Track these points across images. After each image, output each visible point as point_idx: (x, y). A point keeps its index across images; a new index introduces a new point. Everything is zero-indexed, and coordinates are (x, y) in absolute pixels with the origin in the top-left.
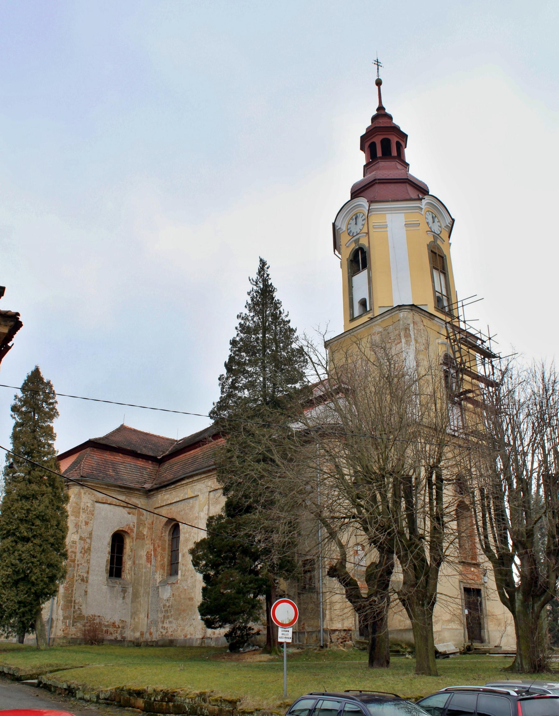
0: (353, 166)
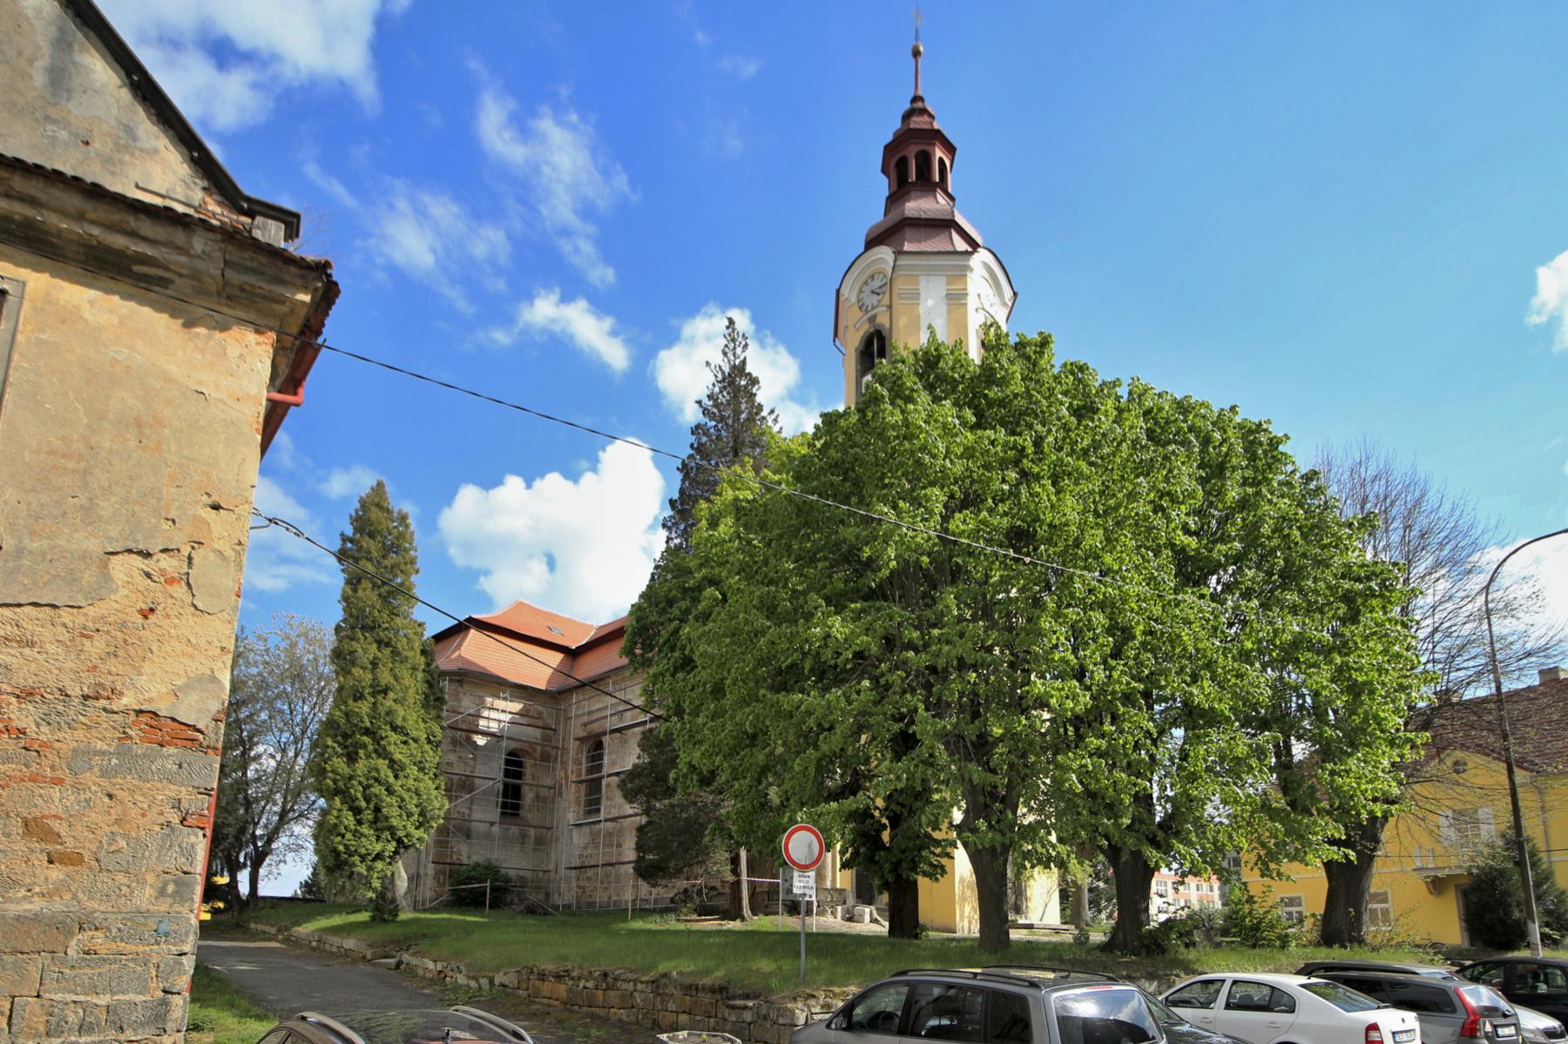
0: (870, 196)
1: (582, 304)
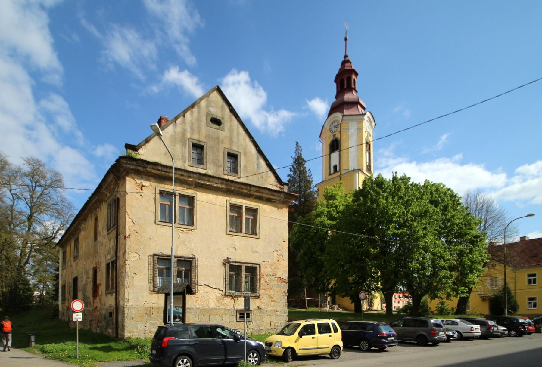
1: (186, 73)
